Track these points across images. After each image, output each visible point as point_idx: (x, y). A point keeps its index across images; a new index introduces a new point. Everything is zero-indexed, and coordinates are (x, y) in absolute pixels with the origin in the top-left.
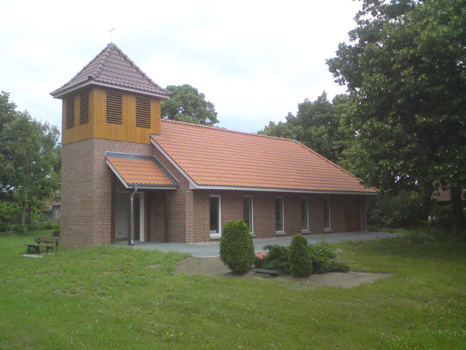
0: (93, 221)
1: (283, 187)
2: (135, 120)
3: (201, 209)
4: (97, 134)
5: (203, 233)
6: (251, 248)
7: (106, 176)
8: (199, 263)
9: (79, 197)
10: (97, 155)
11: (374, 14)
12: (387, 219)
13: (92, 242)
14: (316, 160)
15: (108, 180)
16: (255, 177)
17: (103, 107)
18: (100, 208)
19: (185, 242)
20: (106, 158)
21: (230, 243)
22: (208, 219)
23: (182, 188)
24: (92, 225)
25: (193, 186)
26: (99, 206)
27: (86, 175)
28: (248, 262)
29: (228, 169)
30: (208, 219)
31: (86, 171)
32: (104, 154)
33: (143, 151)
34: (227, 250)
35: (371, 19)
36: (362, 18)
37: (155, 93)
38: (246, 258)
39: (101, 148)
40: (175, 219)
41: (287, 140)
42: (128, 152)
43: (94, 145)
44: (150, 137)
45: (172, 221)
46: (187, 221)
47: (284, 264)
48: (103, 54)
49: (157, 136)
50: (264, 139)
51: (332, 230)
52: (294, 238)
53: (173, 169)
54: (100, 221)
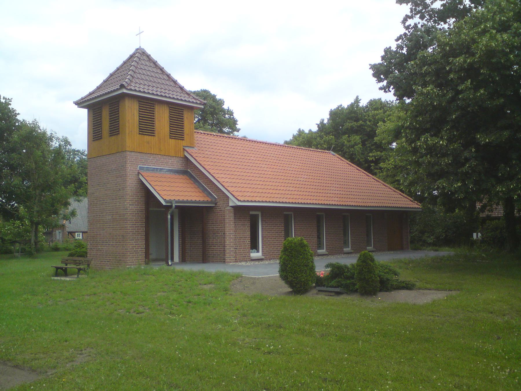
0: (126, 240)
1: (326, 202)
2: (168, 131)
3: (241, 227)
4: (129, 146)
5: (243, 253)
6: (313, 266)
7: (139, 192)
8: (254, 283)
9: (109, 215)
10: (130, 170)
11: (422, 18)
12: (429, 237)
13: (125, 263)
14: (355, 173)
15: (141, 197)
16: (296, 193)
17: (135, 118)
18: (133, 227)
19: (224, 262)
20: (139, 173)
21: (291, 261)
22: (248, 237)
23: (221, 204)
24: (126, 245)
25: (233, 202)
26: (132, 225)
27: (118, 191)
28: (309, 281)
29: (268, 183)
30: (248, 237)
31: (117, 186)
32: (137, 168)
33: (176, 164)
34: (287, 268)
35: (419, 23)
36: (411, 22)
37: (189, 102)
38: (307, 276)
39: (133, 162)
40: (213, 238)
41: (323, 152)
42: (161, 167)
43: (126, 159)
44: (184, 149)
45: (210, 240)
46: (228, 240)
47: (348, 282)
48: (132, 59)
49: (191, 149)
50: (300, 151)
51: (375, 248)
52: (360, 256)
53: (210, 184)
54: (133, 240)
